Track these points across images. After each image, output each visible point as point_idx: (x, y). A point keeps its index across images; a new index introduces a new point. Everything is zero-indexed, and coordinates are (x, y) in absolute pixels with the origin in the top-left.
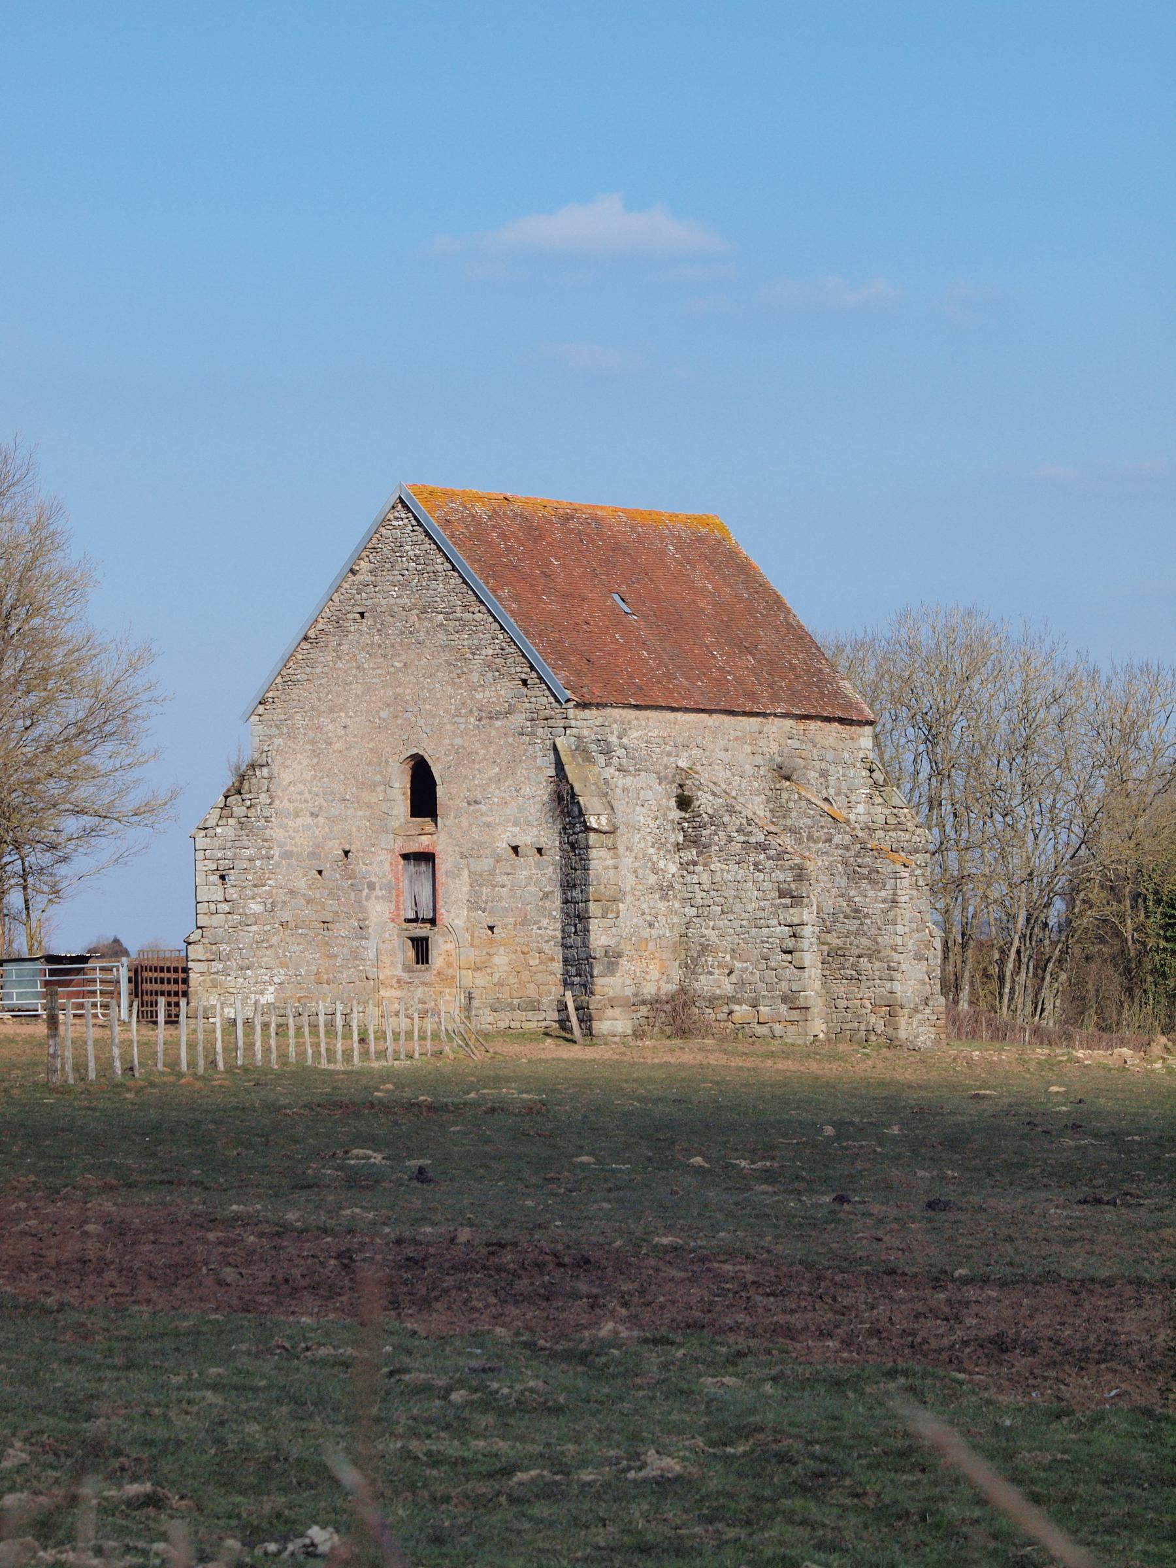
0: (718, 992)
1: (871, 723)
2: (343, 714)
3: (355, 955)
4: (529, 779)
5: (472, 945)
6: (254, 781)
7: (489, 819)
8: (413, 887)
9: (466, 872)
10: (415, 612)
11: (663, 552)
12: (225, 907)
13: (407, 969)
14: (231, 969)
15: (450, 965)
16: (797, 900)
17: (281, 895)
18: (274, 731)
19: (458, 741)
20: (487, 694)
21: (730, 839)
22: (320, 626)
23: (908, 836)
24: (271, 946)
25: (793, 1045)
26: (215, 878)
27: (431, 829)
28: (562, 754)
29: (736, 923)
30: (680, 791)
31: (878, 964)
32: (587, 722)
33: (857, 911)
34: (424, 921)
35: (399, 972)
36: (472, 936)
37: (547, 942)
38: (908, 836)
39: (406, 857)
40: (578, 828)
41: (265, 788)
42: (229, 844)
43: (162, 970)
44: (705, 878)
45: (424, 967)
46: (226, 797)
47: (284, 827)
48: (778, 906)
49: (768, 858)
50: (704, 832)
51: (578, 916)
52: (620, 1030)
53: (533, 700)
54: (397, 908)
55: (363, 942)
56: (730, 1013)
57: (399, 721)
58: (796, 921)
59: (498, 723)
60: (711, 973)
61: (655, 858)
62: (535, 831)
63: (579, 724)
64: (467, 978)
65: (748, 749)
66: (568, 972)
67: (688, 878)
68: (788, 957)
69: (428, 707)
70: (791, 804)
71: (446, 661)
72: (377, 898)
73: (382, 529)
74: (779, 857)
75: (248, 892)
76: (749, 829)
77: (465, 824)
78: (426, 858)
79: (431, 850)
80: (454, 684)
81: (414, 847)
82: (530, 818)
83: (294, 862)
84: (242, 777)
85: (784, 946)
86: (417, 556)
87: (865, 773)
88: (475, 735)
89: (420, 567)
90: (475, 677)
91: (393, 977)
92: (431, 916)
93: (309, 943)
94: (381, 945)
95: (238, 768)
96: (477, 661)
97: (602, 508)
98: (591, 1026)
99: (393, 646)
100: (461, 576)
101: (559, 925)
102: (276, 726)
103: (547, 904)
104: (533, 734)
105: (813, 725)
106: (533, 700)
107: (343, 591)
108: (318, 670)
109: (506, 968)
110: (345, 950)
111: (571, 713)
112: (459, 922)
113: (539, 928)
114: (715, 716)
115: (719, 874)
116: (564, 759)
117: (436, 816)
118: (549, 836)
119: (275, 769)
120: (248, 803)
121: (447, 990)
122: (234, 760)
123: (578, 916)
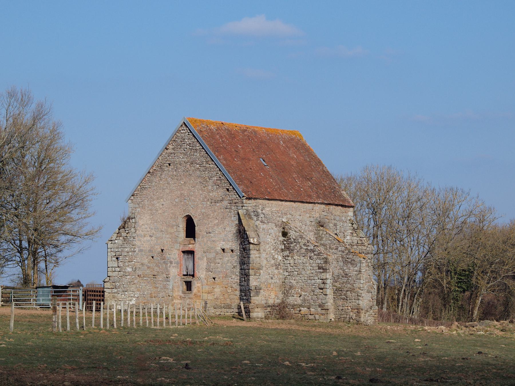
0: (296, 303)
3: (165, 287)
5: (207, 285)
6: (129, 224)
7: (214, 239)
8: (186, 263)
9: (205, 258)
10: (189, 163)
11: (279, 144)
12: (118, 269)
13: (183, 293)
15: (199, 291)
16: (325, 270)
17: (138, 265)
18: (137, 206)
19: (203, 211)
21: (301, 248)
22: (154, 168)
26: (114, 259)
27: (193, 242)
29: (303, 278)
31: (354, 294)
32: (250, 204)
33: (346, 275)
34: (190, 275)
35: (180, 294)
36: (207, 281)
38: (365, 248)
39: (184, 252)
42: (120, 246)
43: (95, 291)
44: (292, 261)
46: (119, 229)
47: (140, 241)
48: (318, 272)
50: (292, 245)
54: (180, 270)
55: (168, 283)
56: (300, 311)
57: (182, 203)
58: (324, 278)
59: (218, 204)
60: (293, 296)
61: (274, 254)
62: (230, 244)
63: (247, 205)
64: (205, 296)
65: (308, 215)
67: (286, 262)
68: (321, 291)
70: (323, 236)
72: (173, 267)
73: (177, 134)
74: (319, 254)
75: (127, 264)
76: (308, 244)
77: (205, 241)
78: (191, 253)
80: (202, 190)
81: (187, 249)
83: (143, 253)
84: (125, 222)
87: (350, 225)
90: (210, 187)
92: (192, 274)
93: (148, 282)
95: (124, 219)
96: (211, 182)
97: (257, 127)
101: (239, 278)
103: (235, 270)
104: (230, 208)
105: (332, 207)
108: (153, 184)
111: (244, 201)
114: (296, 203)
118: (235, 245)
119: (137, 219)
120: (127, 232)
122: (122, 216)
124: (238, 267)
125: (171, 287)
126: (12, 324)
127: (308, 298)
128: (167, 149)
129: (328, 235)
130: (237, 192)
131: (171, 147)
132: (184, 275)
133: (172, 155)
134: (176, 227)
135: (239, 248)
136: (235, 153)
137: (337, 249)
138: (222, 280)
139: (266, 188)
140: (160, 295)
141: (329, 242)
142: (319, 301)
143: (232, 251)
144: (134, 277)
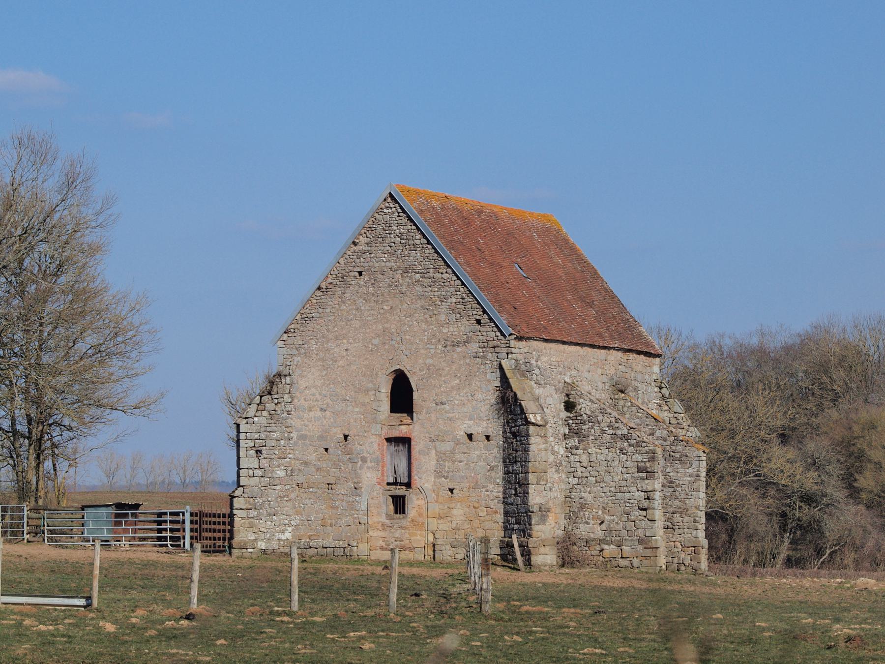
0: (592, 536)
1: (659, 356)
2: (345, 341)
3: (351, 506)
4: (481, 388)
5: (437, 502)
6: (280, 386)
7: (451, 415)
9: (434, 451)
10: (400, 272)
11: (532, 237)
12: (259, 472)
13: (389, 517)
14: (263, 515)
15: (420, 515)
16: (650, 474)
17: (297, 465)
18: (295, 352)
20: (451, 329)
21: (603, 432)
22: (329, 280)
23: (684, 432)
24: (290, 500)
25: (647, 573)
26: (252, 452)
27: (409, 421)
28: (506, 371)
29: (606, 489)
30: (566, 399)
31: (686, 519)
32: (520, 348)
33: (671, 482)
34: (402, 484)
35: (383, 519)
36: (437, 495)
37: (492, 500)
38: (684, 432)
39: (389, 440)
40: (519, 422)
41: (287, 391)
42: (263, 429)
43: (214, 516)
44: (584, 458)
45: (401, 516)
46: (261, 397)
47: (301, 418)
48: (637, 478)
49: (630, 445)
50: (584, 427)
51: (519, 483)
52: (549, 562)
53: (485, 334)
54: (383, 475)
55: (357, 498)
56: (602, 551)
57: (387, 347)
58: (650, 488)
59: (459, 350)
60: (588, 523)
61: (553, 444)
63: (517, 351)
64: (433, 524)
65: (600, 371)
66: (508, 521)
67: (572, 458)
68: (644, 513)
69: (408, 337)
70: (625, 409)
71: (422, 306)
72: (368, 468)
73: (376, 215)
74: (639, 444)
75: (276, 463)
76: (617, 425)
77: (433, 419)
78: (405, 441)
79: (408, 435)
81: (396, 433)
82: (482, 415)
84: (272, 383)
85: (641, 506)
86: (402, 234)
87: (657, 389)
88: (441, 357)
89: (403, 241)
90: (443, 317)
91: (378, 522)
92: (406, 481)
94: (370, 500)
95: (267, 377)
96: (444, 307)
97: (495, 206)
98: (530, 559)
99: (382, 295)
100: (433, 247)
101: (501, 489)
102: (297, 348)
103: (493, 474)
104: (484, 357)
105: (632, 356)
106: (485, 334)
107: (347, 256)
108: (328, 311)
109: (462, 518)
110: (344, 504)
111: (512, 343)
112: (428, 486)
113: (487, 491)
114: (584, 348)
115: (594, 455)
116: (509, 374)
117: (412, 412)
118: (495, 428)
119: (295, 377)
120: (276, 401)
121: (419, 532)
122: (266, 372)
123: (519, 483)
124: (501, 467)
125: (364, 507)
126: (394, 597)
127: (617, 527)
128: (355, 244)
129: (634, 409)
130: (497, 326)
131: (362, 239)
132: (388, 484)
133: (365, 256)
134: (373, 392)
135: (501, 433)
136: (478, 253)
137: (652, 434)
138: (467, 494)
139: (539, 320)
140: (343, 521)
141: (638, 421)
142: (640, 532)
143: (488, 438)
144: (288, 487)
